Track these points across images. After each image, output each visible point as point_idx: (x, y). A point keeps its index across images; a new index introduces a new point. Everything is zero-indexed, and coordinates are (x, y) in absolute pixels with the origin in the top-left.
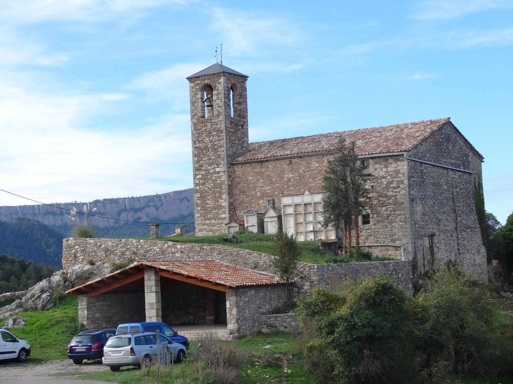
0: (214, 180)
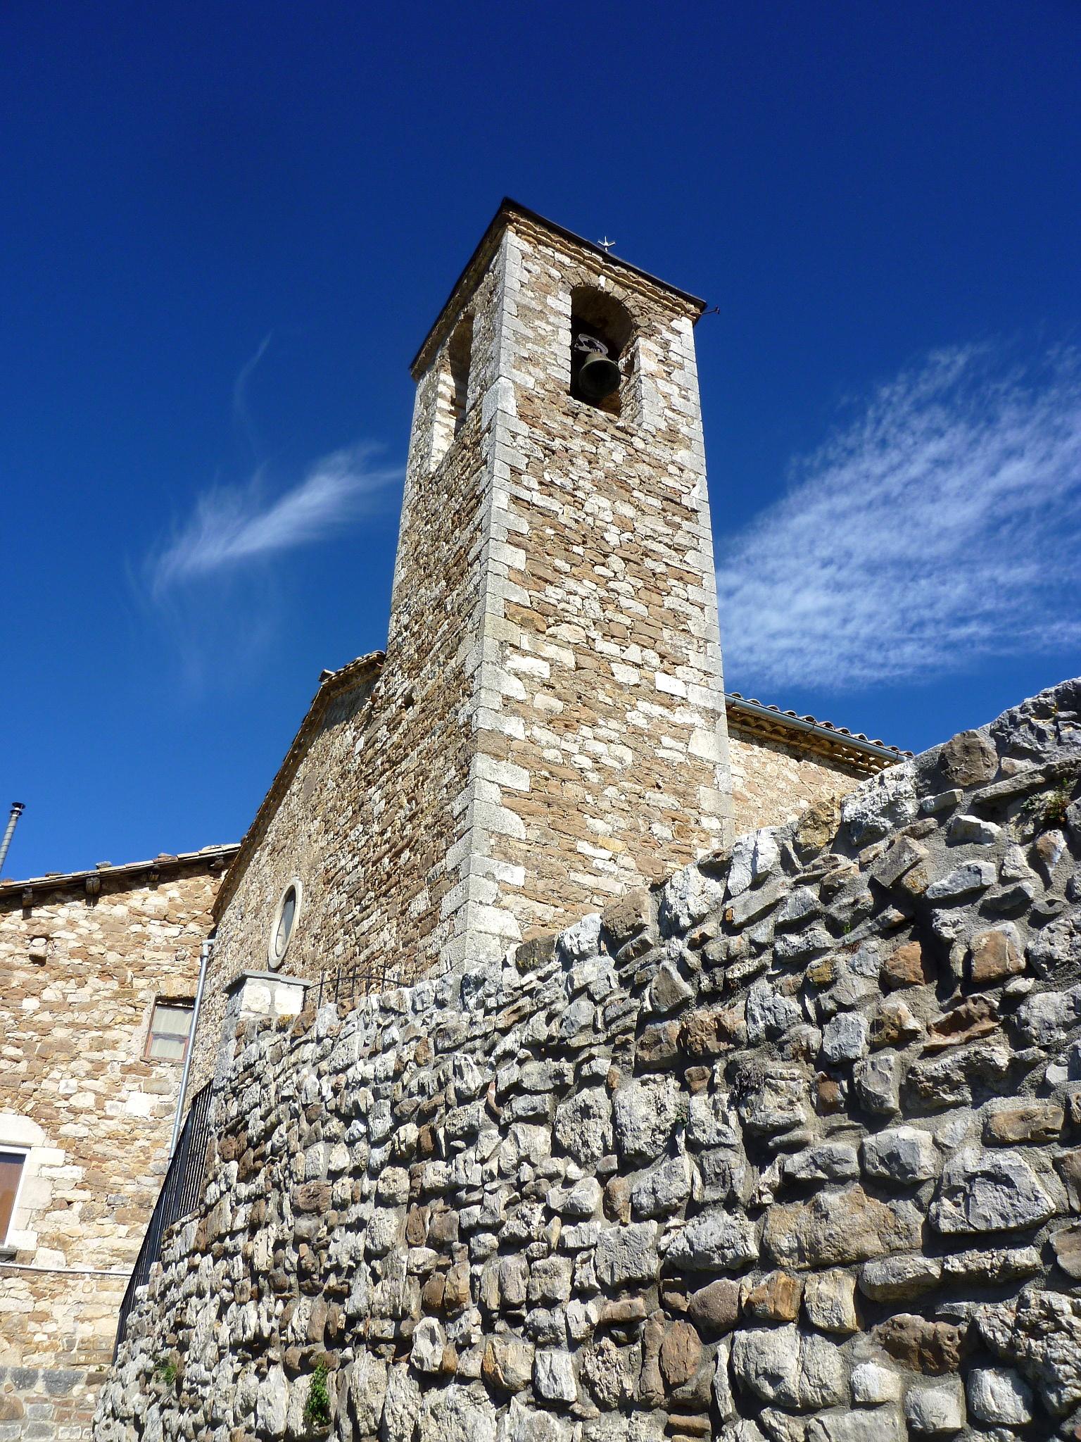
0: (637, 732)
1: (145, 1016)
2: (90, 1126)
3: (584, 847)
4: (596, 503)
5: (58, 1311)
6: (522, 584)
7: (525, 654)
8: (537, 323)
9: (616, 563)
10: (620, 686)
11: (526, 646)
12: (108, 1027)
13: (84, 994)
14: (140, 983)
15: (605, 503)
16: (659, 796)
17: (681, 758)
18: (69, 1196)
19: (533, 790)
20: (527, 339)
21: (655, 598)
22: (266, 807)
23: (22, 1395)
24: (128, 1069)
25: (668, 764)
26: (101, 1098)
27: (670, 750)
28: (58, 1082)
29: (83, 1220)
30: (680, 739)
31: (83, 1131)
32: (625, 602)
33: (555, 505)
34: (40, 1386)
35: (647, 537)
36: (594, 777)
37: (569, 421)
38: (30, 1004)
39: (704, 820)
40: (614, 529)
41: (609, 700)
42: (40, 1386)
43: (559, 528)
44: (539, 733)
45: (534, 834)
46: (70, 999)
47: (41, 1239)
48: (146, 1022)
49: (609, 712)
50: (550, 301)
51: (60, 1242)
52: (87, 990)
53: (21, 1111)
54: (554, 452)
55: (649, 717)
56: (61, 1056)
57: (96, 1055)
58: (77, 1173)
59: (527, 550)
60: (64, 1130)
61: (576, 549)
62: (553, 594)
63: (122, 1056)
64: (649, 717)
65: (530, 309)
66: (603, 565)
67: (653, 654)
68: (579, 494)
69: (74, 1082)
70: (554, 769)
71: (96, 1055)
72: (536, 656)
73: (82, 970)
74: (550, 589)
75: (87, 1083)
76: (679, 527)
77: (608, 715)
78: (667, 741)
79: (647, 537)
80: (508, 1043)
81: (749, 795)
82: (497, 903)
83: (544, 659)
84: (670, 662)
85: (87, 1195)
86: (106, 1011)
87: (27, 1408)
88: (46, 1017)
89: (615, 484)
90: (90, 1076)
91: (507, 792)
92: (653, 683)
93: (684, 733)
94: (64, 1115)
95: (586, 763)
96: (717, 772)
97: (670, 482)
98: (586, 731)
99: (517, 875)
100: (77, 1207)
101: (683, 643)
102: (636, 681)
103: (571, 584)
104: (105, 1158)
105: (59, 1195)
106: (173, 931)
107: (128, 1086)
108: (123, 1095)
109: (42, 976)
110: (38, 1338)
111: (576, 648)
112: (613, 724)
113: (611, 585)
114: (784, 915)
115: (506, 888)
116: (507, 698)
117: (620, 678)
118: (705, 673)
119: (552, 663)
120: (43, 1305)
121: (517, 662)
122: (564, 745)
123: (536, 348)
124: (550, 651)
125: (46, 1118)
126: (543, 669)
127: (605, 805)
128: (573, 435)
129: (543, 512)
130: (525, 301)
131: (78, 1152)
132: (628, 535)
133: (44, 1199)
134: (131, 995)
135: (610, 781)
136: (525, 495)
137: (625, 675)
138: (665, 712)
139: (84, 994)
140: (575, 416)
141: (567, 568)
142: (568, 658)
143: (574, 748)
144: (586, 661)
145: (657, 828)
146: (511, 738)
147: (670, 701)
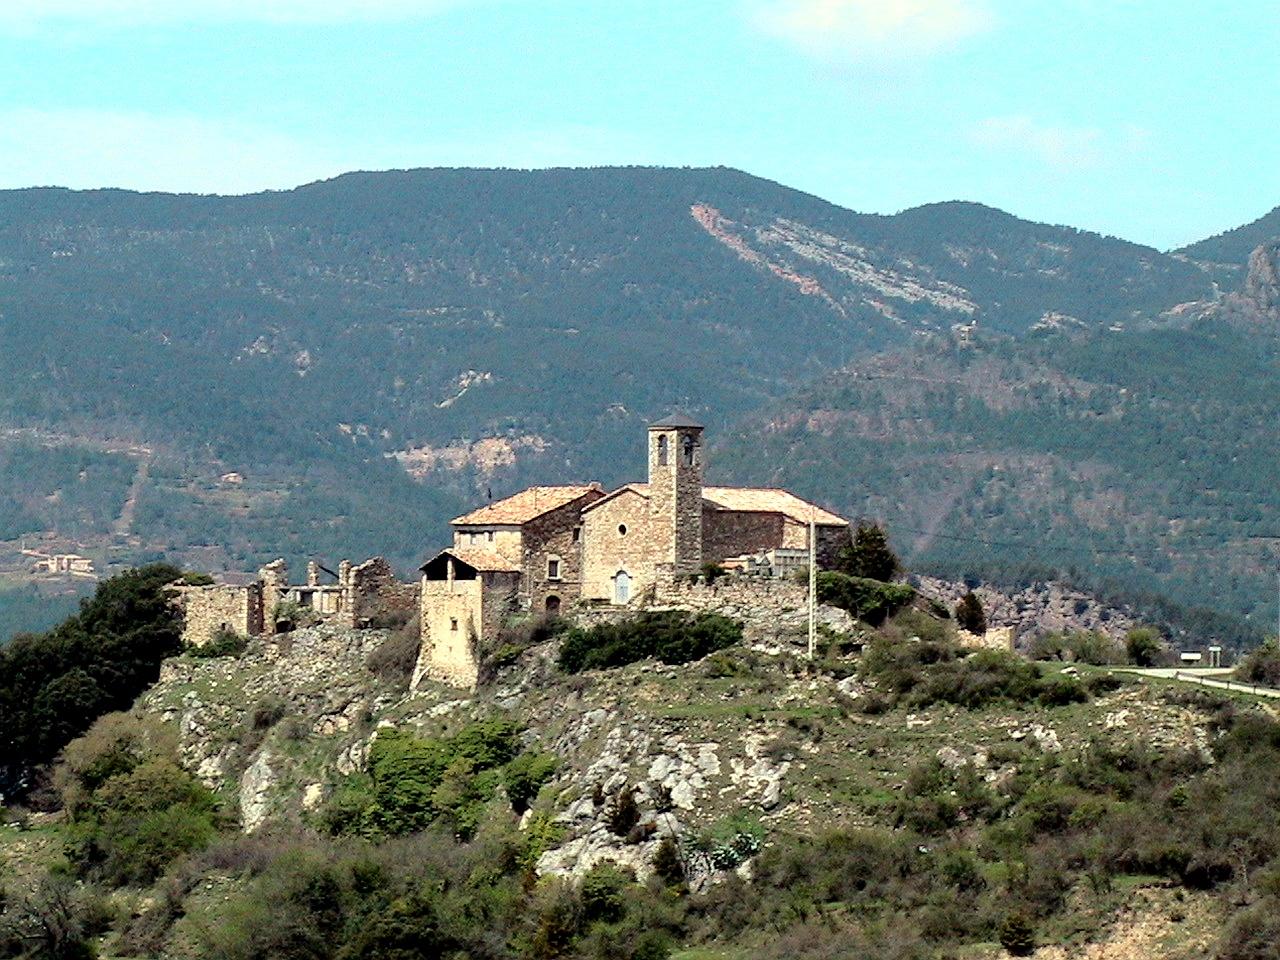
4: (688, 486)
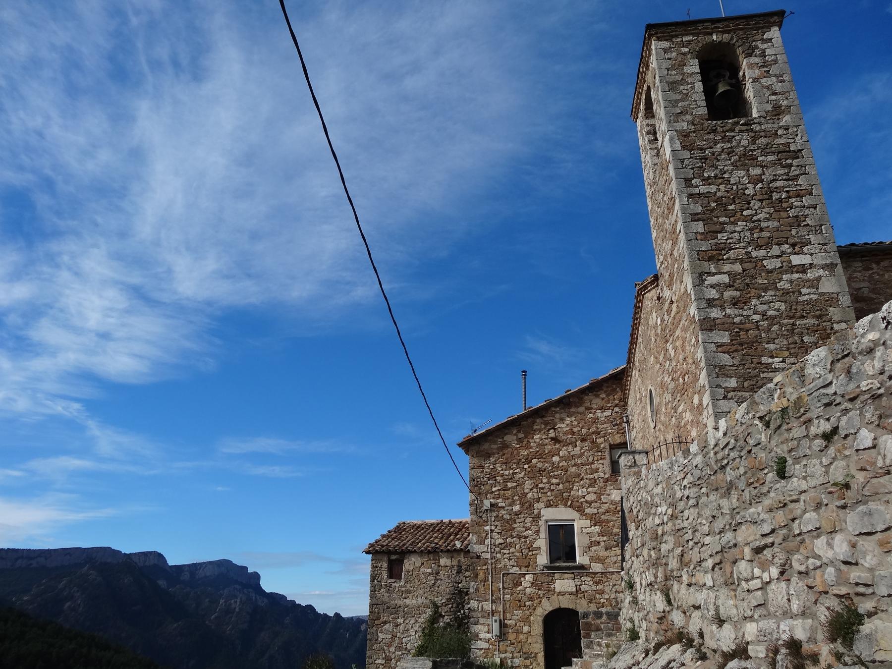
0: (786, 293)
1: (607, 454)
2: (598, 508)
3: (764, 360)
5: (607, 589)
6: (705, 239)
7: (714, 274)
8: (682, 88)
9: (755, 204)
10: (771, 272)
11: (713, 270)
12: (592, 463)
13: (577, 451)
14: (600, 440)
15: (743, 173)
16: (805, 321)
17: (816, 297)
18: (598, 539)
19: (732, 341)
20: (677, 101)
21: (784, 214)
22: (630, 349)
23: (598, 621)
24: (607, 480)
25: (807, 303)
26: (599, 495)
27: (807, 295)
28: (579, 491)
29: (607, 549)
30: (813, 287)
31: (595, 511)
32: (763, 224)
33: (713, 188)
34: (605, 617)
35: (772, 181)
36: (765, 323)
37: (711, 136)
38: (556, 459)
39: (836, 327)
40: (749, 186)
41: (766, 281)
42: (605, 617)
43: (719, 201)
44: (728, 311)
45: (736, 361)
46: (572, 453)
47: (592, 559)
48: (608, 457)
49: (767, 287)
50: (686, 69)
51: (601, 560)
52: (578, 448)
53: (566, 505)
54: (707, 159)
55: (791, 282)
56: (577, 479)
57: (591, 476)
58: (597, 529)
59: (703, 220)
60: (587, 511)
61: (730, 207)
62: (722, 237)
63: (602, 475)
64: (791, 282)
65: (675, 82)
66: (748, 209)
67: (787, 246)
68: (726, 176)
69: (584, 490)
70: (742, 326)
71: (591, 476)
72: (720, 273)
73: (573, 440)
74: (719, 235)
75: (590, 489)
76: (791, 165)
77: (766, 290)
78: (804, 291)
79: (772, 181)
80: (685, 482)
81: (874, 296)
82: (725, 398)
83: (724, 273)
84: (798, 246)
85: (605, 538)
86: (589, 456)
87: (602, 626)
88: (564, 463)
89: (746, 160)
90: (590, 486)
91: (719, 346)
92: (790, 262)
93: (815, 283)
94: (585, 504)
95: (757, 317)
96: (840, 297)
97: (781, 141)
98: (754, 302)
99: (733, 383)
100: (602, 544)
101: (806, 233)
102: (780, 265)
103: (729, 228)
104: (608, 521)
105: (593, 539)
106: (608, 413)
107: (608, 488)
108: (608, 492)
109: (557, 446)
110: (602, 601)
111: (742, 262)
112: (771, 293)
113: (755, 218)
114: (730, 447)
115: (727, 390)
116: (709, 300)
117: (769, 267)
118: (824, 244)
119: (729, 273)
120: (600, 587)
121: (711, 280)
122: (744, 313)
123: (684, 103)
124: (727, 268)
125: (580, 510)
126: (725, 279)
127: (774, 336)
128: (716, 143)
129: (708, 195)
130: (671, 79)
131: (595, 520)
132: (760, 185)
133: (587, 541)
134: (598, 447)
135: (659, 426)
136: (696, 191)
137: (771, 264)
138: (801, 275)
139: (577, 451)
140: (714, 131)
141: (727, 220)
142: (738, 268)
143: (750, 312)
144: (746, 265)
145: (806, 339)
146: (715, 319)
147: (803, 269)
